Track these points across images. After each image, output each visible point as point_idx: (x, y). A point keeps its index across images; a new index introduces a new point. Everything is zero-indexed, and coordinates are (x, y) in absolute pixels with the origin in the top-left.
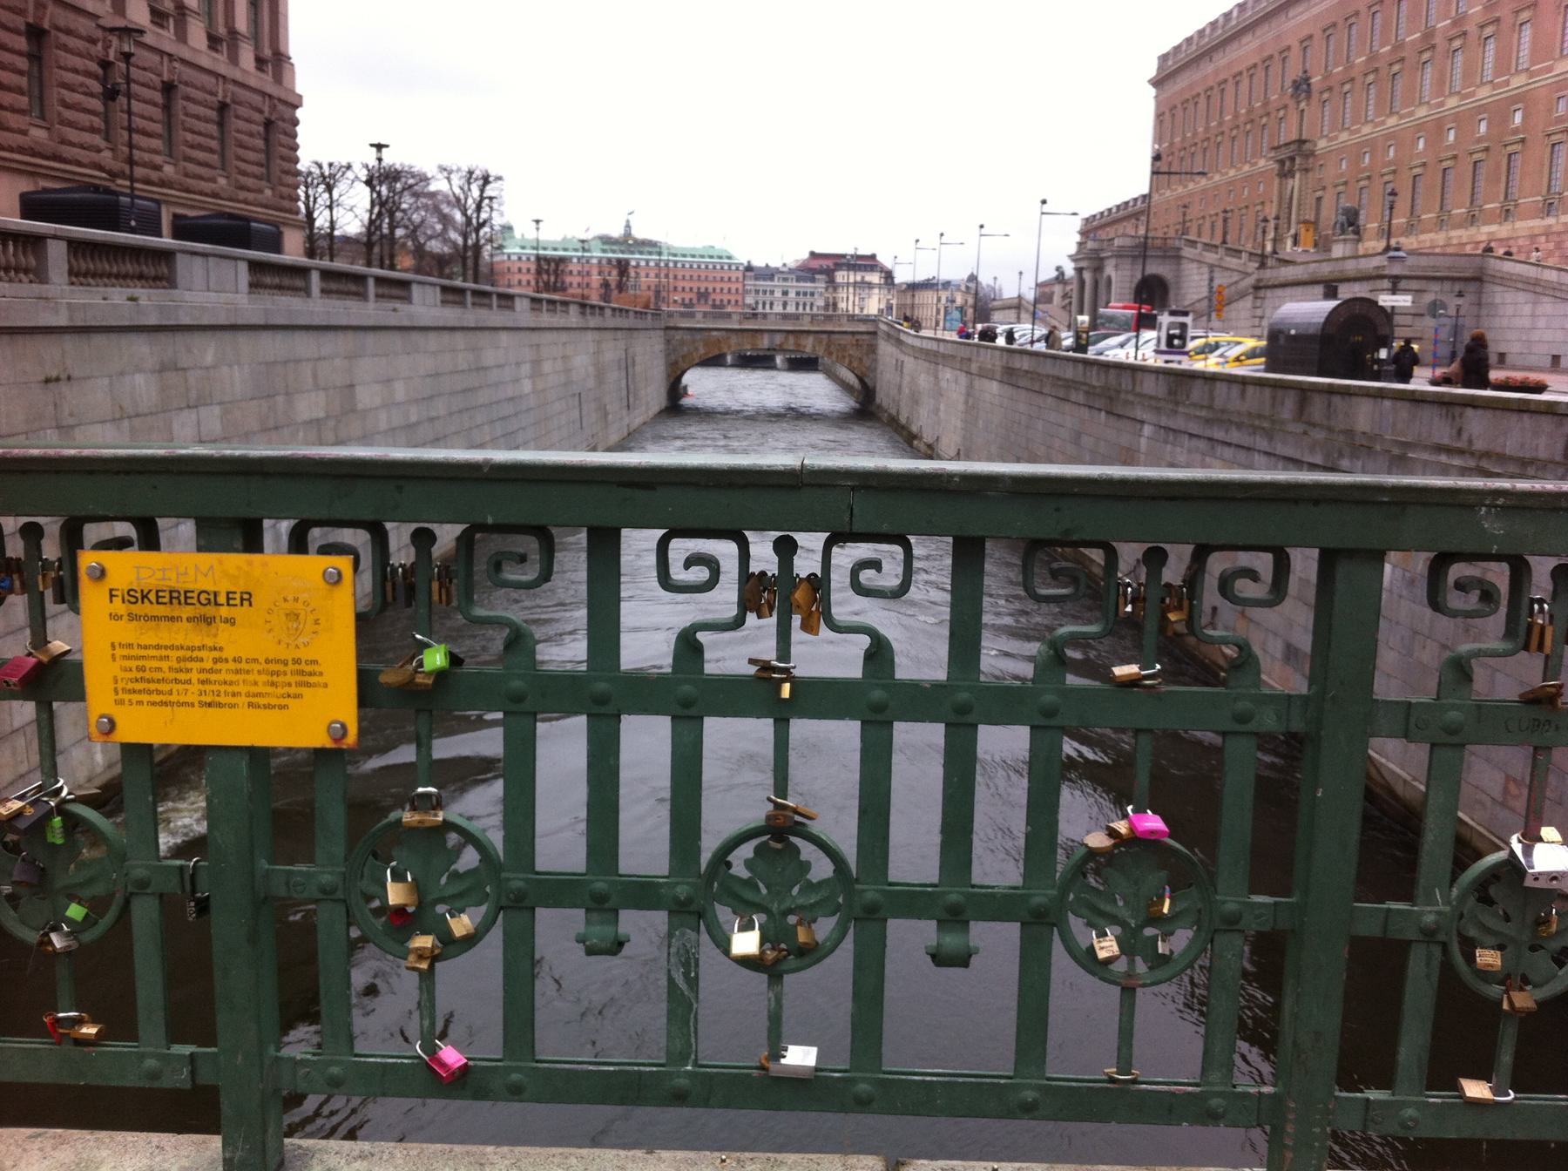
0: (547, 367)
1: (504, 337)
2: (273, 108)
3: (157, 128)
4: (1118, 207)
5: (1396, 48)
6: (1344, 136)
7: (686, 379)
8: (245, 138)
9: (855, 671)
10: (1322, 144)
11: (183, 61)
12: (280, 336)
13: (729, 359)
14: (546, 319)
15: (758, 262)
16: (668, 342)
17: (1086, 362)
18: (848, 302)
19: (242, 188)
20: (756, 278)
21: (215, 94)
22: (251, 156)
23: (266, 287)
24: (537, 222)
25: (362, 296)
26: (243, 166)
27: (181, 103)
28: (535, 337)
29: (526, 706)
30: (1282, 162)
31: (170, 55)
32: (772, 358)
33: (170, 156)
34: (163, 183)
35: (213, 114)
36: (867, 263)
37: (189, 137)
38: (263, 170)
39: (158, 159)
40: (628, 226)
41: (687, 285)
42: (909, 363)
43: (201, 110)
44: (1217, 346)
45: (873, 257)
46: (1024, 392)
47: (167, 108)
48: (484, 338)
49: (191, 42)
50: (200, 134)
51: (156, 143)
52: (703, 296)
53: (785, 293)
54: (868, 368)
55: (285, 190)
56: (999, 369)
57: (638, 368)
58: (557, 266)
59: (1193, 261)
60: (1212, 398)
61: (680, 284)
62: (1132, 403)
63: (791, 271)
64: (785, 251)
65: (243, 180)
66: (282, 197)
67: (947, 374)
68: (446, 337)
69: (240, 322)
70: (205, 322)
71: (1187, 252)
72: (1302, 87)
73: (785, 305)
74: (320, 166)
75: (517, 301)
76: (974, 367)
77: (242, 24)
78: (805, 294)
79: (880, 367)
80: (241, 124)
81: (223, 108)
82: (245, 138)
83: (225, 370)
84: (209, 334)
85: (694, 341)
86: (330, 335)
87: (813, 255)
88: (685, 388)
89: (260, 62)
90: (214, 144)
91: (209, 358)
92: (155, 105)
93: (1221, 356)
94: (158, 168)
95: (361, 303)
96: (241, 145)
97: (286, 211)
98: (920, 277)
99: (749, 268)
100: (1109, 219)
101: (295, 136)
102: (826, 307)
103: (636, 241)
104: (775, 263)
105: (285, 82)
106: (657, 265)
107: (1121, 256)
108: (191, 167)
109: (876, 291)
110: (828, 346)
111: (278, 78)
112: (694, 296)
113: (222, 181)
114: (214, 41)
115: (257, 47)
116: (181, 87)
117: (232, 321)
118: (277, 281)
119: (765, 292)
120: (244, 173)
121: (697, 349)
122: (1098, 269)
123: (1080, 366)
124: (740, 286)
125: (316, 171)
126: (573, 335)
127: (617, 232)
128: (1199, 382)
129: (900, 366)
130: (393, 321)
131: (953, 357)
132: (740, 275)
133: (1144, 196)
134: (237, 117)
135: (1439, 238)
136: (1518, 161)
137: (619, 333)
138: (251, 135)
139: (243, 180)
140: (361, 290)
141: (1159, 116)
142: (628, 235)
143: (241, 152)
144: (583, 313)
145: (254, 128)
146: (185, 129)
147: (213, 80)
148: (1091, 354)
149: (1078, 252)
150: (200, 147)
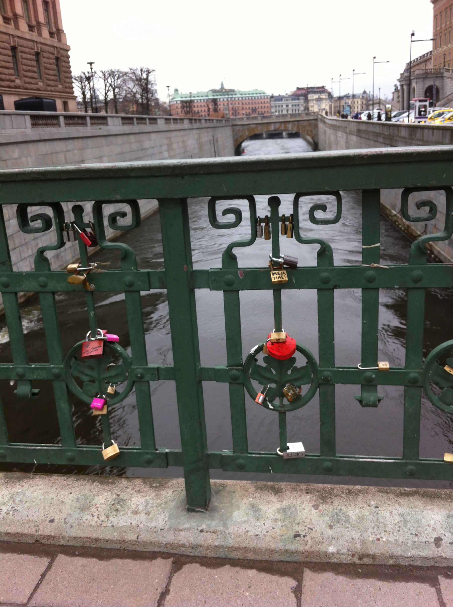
0: (175, 146)
1: (153, 136)
2: (58, 52)
3: (11, 65)
4: (421, 57)
7: (244, 144)
8: (48, 66)
9: (313, 263)
11: (18, 37)
12: (47, 144)
13: (264, 136)
14: (173, 126)
15: (276, 94)
16: (233, 131)
17: (393, 126)
18: (314, 108)
19: (49, 86)
20: (275, 100)
21: (33, 49)
22: (51, 72)
23: (40, 125)
24: (168, 87)
25: (85, 124)
26: (49, 77)
27: (20, 54)
28: (168, 134)
29: (234, 287)
31: (12, 35)
32: (281, 134)
33: (18, 76)
34: (16, 87)
35: (34, 57)
36: (321, 90)
37: (25, 67)
38: (57, 78)
39: (13, 78)
40: (222, 84)
41: (247, 106)
42: (328, 130)
43: (29, 56)
44: (443, 113)
45: (323, 87)
46: (364, 139)
47: (14, 57)
48: (145, 137)
49: (20, 29)
50: (29, 66)
51: (11, 71)
52: (254, 110)
53: (287, 106)
54: (315, 134)
55: (67, 85)
56: (355, 130)
57: (220, 143)
58: (189, 104)
59: (448, 78)
60: (423, 136)
61: (245, 106)
62: (398, 141)
63: (289, 96)
64: (286, 88)
65: (49, 82)
66: (66, 88)
67: (340, 134)
68: (125, 138)
69: (28, 139)
70: (12, 141)
71: (446, 74)
73: (287, 111)
74: (84, 74)
75: (158, 120)
76: (348, 130)
77: (42, 19)
78: (295, 105)
79: (320, 134)
80: (46, 60)
81: (37, 54)
82: (48, 66)
83: (24, 159)
84: (15, 146)
85: (243, 130)
86: (71, 141)
87: (298, 89)
88: (243, 150)
89: (51, 34)
90: (35, 69)
91: (16, 155)
92: (9, 56)
93: (443, 118)
94: (13, 81)
95: (85, 128)
96: (47, 68)
97: (68, 93)
98: (342, 94)
99: (272, 97)
100: (417, 63)
101: (69, 62)
102: (305, 110)
103: (226, 90)
104: (283, 94)
105: (62, 41)
106: (228, 100)
107: (418, 78)
108: (27, 79)
109: (324, 101)
110: (298, 126)
111: (60, 40)
112: (250, 111)
113: (41, 84)
114: (31, 28)
115: (50, 28)
116: (19, 48)
117: (25, 139)
118: (44, 122)
119: (279, 106)
120: (49, 80)
121: (245, 133)
122: (409, 85)
123: (381, 126)
124: (269, 105)
125: (83, 75)
126: (188, 132)
127: (218, 87)
128: (419, 130)
129: (325, 132)
130: (99, 133)
131: (341, 127)
132: (268, 100)
133: (431, 52)
134: (44, 57)
137: (209, 130)
138: (50, 64)
139: (49, 82)
140: (84, 122)
141: (435, 16)
142: (222, 88)
143: (47, 71)
144: (191, 123)
145: (51, 61)
146: (22, 65)
147: (32, 43)
148: (394, 121)
149: (401, 77)
150: (29, 71)
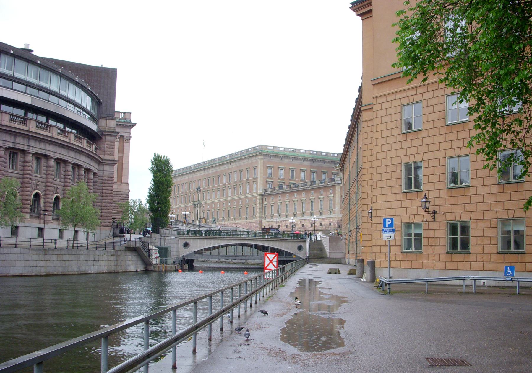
5: (229, 184)
6: (208, 201)
10: (204, 202)
30: (195, 205)
72: (198, 189)
135: (229, 222)
136: (241, 210)
